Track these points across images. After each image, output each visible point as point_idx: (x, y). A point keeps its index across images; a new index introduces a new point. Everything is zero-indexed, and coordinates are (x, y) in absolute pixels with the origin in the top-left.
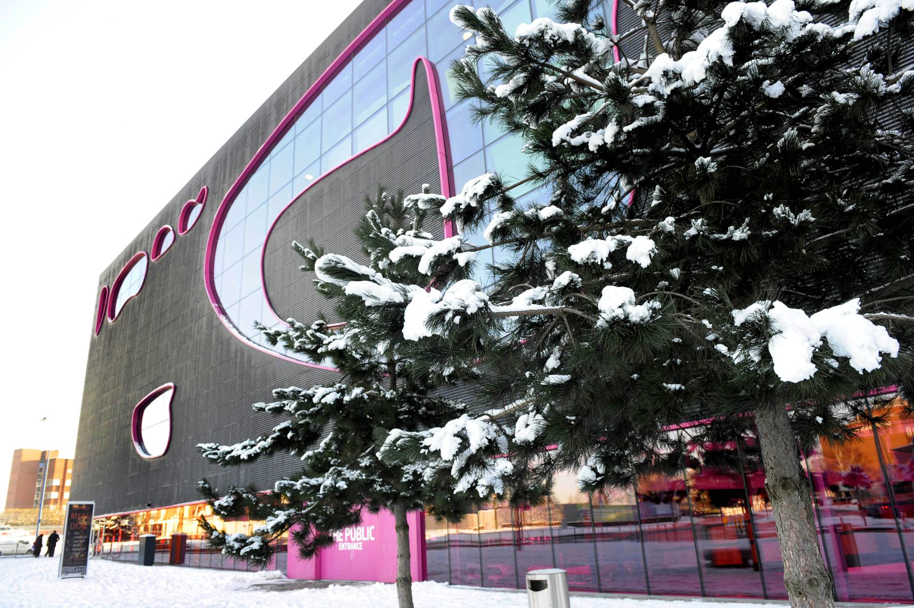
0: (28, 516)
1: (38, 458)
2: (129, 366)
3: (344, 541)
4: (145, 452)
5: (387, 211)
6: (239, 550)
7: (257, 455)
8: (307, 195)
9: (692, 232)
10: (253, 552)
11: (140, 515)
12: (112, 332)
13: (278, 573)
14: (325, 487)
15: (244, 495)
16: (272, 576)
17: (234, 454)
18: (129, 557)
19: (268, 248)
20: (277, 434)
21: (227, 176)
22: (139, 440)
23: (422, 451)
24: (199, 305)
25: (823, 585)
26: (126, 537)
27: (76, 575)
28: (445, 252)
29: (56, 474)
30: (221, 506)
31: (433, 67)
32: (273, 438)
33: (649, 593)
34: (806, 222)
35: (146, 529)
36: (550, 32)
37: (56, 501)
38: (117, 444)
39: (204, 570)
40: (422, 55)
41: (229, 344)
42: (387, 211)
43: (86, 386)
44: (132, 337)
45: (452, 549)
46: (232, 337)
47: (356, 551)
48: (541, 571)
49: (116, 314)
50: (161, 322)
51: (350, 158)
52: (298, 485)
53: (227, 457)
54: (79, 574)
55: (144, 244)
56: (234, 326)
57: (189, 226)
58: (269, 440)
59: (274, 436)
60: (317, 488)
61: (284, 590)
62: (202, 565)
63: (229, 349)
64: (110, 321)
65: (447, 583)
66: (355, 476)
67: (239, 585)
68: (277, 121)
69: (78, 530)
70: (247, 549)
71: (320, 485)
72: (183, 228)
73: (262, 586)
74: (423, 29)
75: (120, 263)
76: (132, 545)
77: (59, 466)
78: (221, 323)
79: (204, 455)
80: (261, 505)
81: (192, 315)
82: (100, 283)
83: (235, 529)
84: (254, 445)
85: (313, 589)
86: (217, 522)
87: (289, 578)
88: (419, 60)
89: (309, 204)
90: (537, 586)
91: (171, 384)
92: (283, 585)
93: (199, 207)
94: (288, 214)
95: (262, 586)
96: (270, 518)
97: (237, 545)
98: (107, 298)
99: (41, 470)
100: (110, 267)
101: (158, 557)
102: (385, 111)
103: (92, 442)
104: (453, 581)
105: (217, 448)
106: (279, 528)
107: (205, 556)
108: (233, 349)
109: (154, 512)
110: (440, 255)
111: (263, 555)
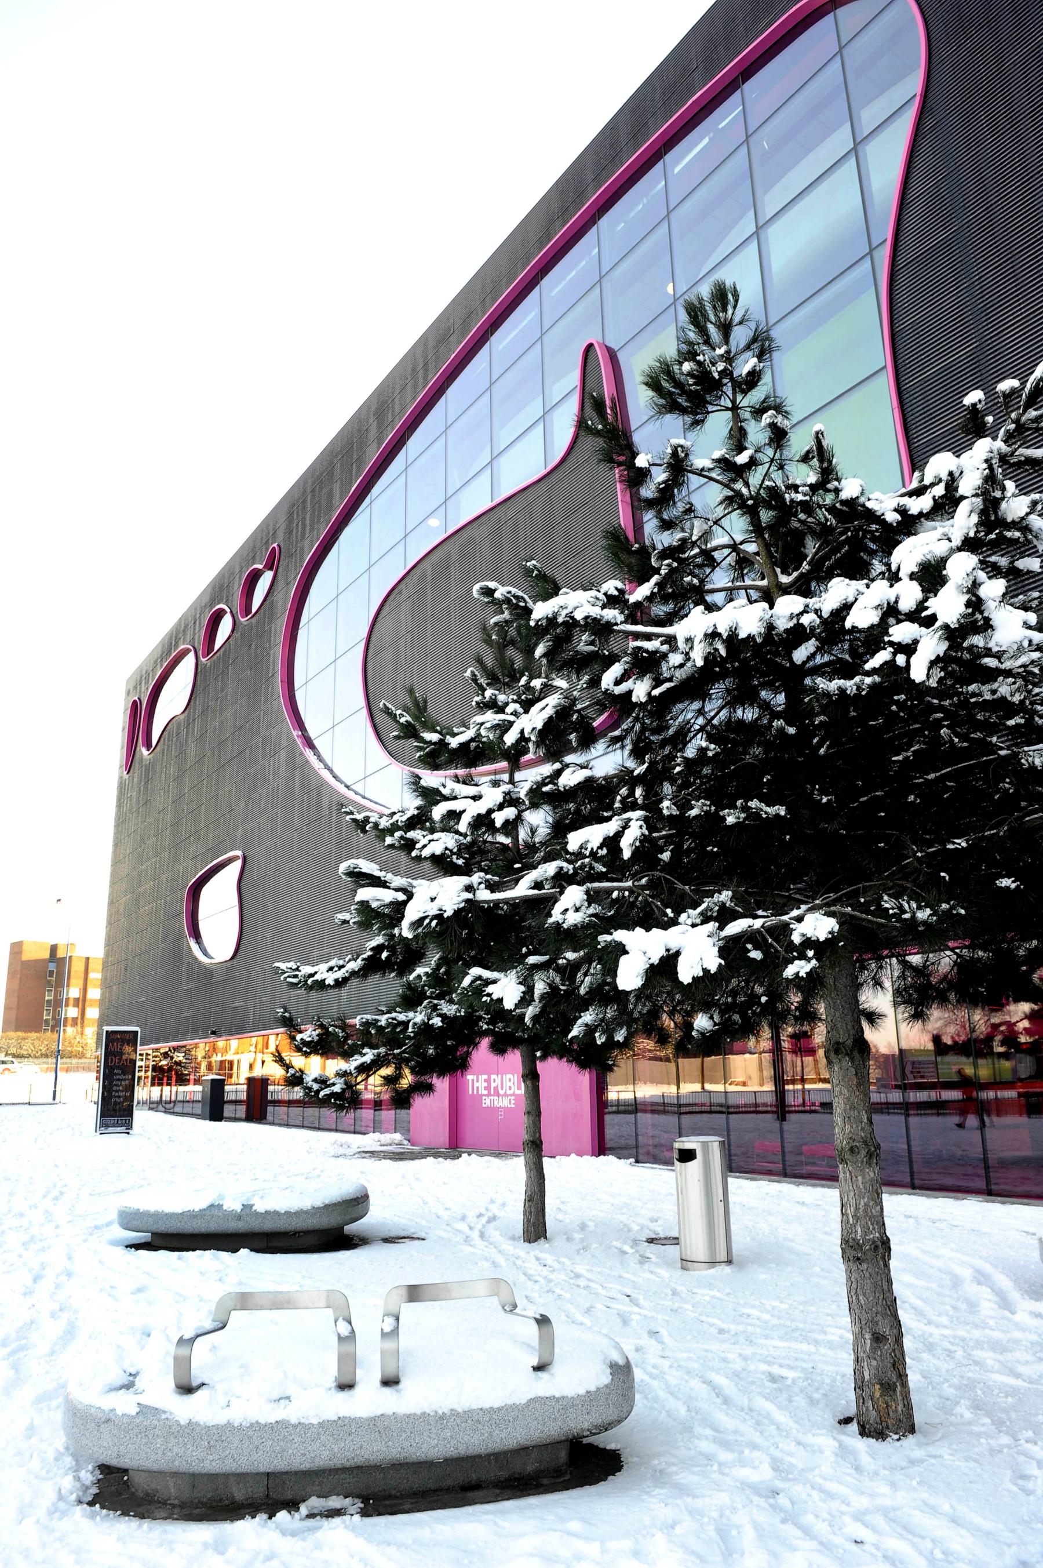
0: (36, 1043)
1: (46, 955)
2: (176, 824)
3: (489, 1095)
4: (205, 953)
5: (512, 642)
6: (318, 1092)
7: (345, 980)
8: (427, 565)
9: (693, 813)
10: (333, 1095)
11: (200, 1048)
12: (149, 771)
13: (397, 1137)
14: (415, 1024)
15: (331, 1029)
16: (388, 1141)
17: (317, 977)
18: (188, 1108)
19: (371, 645)
20: (370, 953)
21: (308, 528)
22: (196, 935)
23: (484, 999)
24: (274, 732)
25: (863, 1153)
26: (182, 1080)
27: (119, 1129)
28: (483, 811)
29: (73, 981)
30: (304, 1043)
31: (612, 356)
32: (363, 960)
33: (913, 1187)
34: (777, 815)
35: (210, 1067)
36: (564, 613)
37: (75, 1021)
38: (164, 940)
39: (294, 1130)
40: (593, 336)
41: (319, 794)
42: (512, 642)
43: (115, 852)
44: (179, 778)
45: (683, 1116)
46: (323, 783)
47: (506, 1109)
48: (692, 1138)
49: (154, 744)
50: (219, 757)
51: (489, 505)
52: (383, 1020)
53: (310, 982)
54: (123, 1129)
55: (190, 633)
56: (327, 767)
57: (255, 606)
58: (359, 962)
59: (364, 956)
60: (406, 1024)
61: (401, 1159)
62: (291, 1122)
63: (319, 802)
64: (145, 752)
65: (632, 1160)
66: (453, 1012)
67: (341, 1151)
68: (380, 441)
69: (119, 1068)
70: (327, 1091)
71: (409, 1021)
72: (247, 610)
73: (372, 1154)
74: (597, 290)
75: (156, 662)
76: (193, 1090)
77: (78, 967)
78: (307, 762)
79: (282, 978)
80: (350, 1042)
81: (264, 749)
82: (128, 693)
83: (314, 1066)
84: (343, 966)
85: (440, 1159)
86: (298, 1061)
87: (412, 1145)
88: (590, 346)
89: (429, 578)
90: (687, 1156)
91: (239, 853)
92: (402, 1153)
93: (267, 577)
94: (400, 593)
95: (372, 1154)
96: (356, 1057)
97: (316, 1087)
98: (140, 716)
99: (51, 973)
100: (140, 668)
101: (228, 1110)
102: (540, 427)
103: (128, 936)
104: (641, 1158)
105: (297, 969)
106: (365, 1069)
107: (295, 1111)
108: (325, 803)
109: (221, 1044)
110: (479, 815)
111: (348, 1100)
